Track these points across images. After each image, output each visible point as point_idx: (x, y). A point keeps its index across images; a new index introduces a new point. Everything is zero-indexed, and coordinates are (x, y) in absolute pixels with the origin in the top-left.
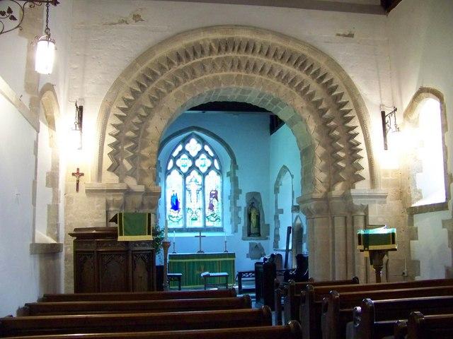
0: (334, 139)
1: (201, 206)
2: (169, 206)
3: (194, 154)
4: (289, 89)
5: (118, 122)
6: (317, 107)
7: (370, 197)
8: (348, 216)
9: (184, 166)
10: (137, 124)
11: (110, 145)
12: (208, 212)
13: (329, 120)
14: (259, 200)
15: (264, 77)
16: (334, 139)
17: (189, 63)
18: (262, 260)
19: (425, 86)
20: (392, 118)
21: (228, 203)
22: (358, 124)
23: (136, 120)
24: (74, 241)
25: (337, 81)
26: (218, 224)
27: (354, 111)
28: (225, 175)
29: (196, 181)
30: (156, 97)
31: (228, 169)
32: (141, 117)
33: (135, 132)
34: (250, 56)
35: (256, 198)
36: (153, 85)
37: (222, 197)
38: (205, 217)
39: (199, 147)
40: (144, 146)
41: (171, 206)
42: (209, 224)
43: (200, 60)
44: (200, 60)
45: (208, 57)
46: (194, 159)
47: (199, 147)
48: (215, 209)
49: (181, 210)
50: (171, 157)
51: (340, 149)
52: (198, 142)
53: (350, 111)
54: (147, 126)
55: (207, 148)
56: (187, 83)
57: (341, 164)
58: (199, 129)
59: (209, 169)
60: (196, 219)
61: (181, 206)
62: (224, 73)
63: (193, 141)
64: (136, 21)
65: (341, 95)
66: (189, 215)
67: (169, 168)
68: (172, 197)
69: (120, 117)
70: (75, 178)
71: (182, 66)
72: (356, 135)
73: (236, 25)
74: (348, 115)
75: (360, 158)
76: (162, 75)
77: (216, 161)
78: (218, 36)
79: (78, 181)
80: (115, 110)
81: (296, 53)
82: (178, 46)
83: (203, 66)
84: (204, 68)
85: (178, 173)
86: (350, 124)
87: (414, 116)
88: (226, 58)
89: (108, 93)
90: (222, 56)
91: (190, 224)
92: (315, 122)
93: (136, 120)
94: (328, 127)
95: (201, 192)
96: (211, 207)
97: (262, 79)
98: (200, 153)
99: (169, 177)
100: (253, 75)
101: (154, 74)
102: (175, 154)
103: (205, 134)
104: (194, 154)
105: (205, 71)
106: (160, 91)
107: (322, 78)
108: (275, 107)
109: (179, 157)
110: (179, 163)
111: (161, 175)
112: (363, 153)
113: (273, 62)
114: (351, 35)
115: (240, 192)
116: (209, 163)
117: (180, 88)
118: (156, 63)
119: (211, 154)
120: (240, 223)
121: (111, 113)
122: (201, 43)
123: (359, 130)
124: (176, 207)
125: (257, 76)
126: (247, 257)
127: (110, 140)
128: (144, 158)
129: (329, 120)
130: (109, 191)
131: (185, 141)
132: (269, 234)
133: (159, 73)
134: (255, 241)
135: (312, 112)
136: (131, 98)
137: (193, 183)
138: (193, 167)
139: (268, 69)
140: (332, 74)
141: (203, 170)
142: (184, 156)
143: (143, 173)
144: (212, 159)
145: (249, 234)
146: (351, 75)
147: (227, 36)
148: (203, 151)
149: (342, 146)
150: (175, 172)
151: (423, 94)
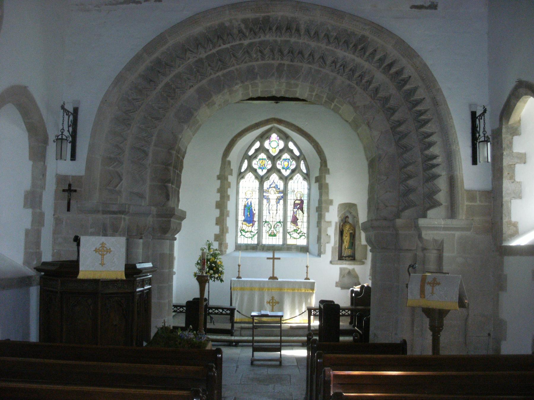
2: (241, 217)
3: (273, 153)
4: (348, 82)
9: (262, 168)
12: (290, 227)
13: (400, 123)
15: (315, 67)
18: (357, 288)
19: (524, 78)
20: (482, 121)
24: (41, 277)
25: (409, 71)
26: (303, 242)
28: (313, 180)
31: (316, 173)
37: (308, 209)
38: (285, 232)
39: (282, 145)
46: (273, 159)
47: (282, 145)
48: (299, 224)
49: (256, 224)
50: (246, 156)
55: (291, 145)
58: (280, 121)
59: (293, 171)
60: (275, 235)
61: (256, 219)
62: (260, 62)
65: (415, 90)
66: (265, 228)
68: (245, 206)
82: (197, 30)
85: (254, 177)
91: (267, 240)
95: (282, 202)
96: (295, 220)
98: (281, 151)
102: (251, 153)
103: (288, 128)
107: (390, 66)
108: (333, 104)
109: (256, 157)
110: (255, 164)
111: (232, 179)
112: (441, 171)
113: (323, 46)
119: (297, 153)
122: (227, 24)
125: (306, 66)
126: (337, 286)
129: (400, 123)
132: (366, 259)
134: (348, 266)
137: (272, 191)
138: (274, 169)
140: (404, 62)
142: (263, 156)
144: (297, 159)
145: (341, 258)
146: (429, 63)
148: (285, 149)
150: (250, 176)
151: (521, 90)
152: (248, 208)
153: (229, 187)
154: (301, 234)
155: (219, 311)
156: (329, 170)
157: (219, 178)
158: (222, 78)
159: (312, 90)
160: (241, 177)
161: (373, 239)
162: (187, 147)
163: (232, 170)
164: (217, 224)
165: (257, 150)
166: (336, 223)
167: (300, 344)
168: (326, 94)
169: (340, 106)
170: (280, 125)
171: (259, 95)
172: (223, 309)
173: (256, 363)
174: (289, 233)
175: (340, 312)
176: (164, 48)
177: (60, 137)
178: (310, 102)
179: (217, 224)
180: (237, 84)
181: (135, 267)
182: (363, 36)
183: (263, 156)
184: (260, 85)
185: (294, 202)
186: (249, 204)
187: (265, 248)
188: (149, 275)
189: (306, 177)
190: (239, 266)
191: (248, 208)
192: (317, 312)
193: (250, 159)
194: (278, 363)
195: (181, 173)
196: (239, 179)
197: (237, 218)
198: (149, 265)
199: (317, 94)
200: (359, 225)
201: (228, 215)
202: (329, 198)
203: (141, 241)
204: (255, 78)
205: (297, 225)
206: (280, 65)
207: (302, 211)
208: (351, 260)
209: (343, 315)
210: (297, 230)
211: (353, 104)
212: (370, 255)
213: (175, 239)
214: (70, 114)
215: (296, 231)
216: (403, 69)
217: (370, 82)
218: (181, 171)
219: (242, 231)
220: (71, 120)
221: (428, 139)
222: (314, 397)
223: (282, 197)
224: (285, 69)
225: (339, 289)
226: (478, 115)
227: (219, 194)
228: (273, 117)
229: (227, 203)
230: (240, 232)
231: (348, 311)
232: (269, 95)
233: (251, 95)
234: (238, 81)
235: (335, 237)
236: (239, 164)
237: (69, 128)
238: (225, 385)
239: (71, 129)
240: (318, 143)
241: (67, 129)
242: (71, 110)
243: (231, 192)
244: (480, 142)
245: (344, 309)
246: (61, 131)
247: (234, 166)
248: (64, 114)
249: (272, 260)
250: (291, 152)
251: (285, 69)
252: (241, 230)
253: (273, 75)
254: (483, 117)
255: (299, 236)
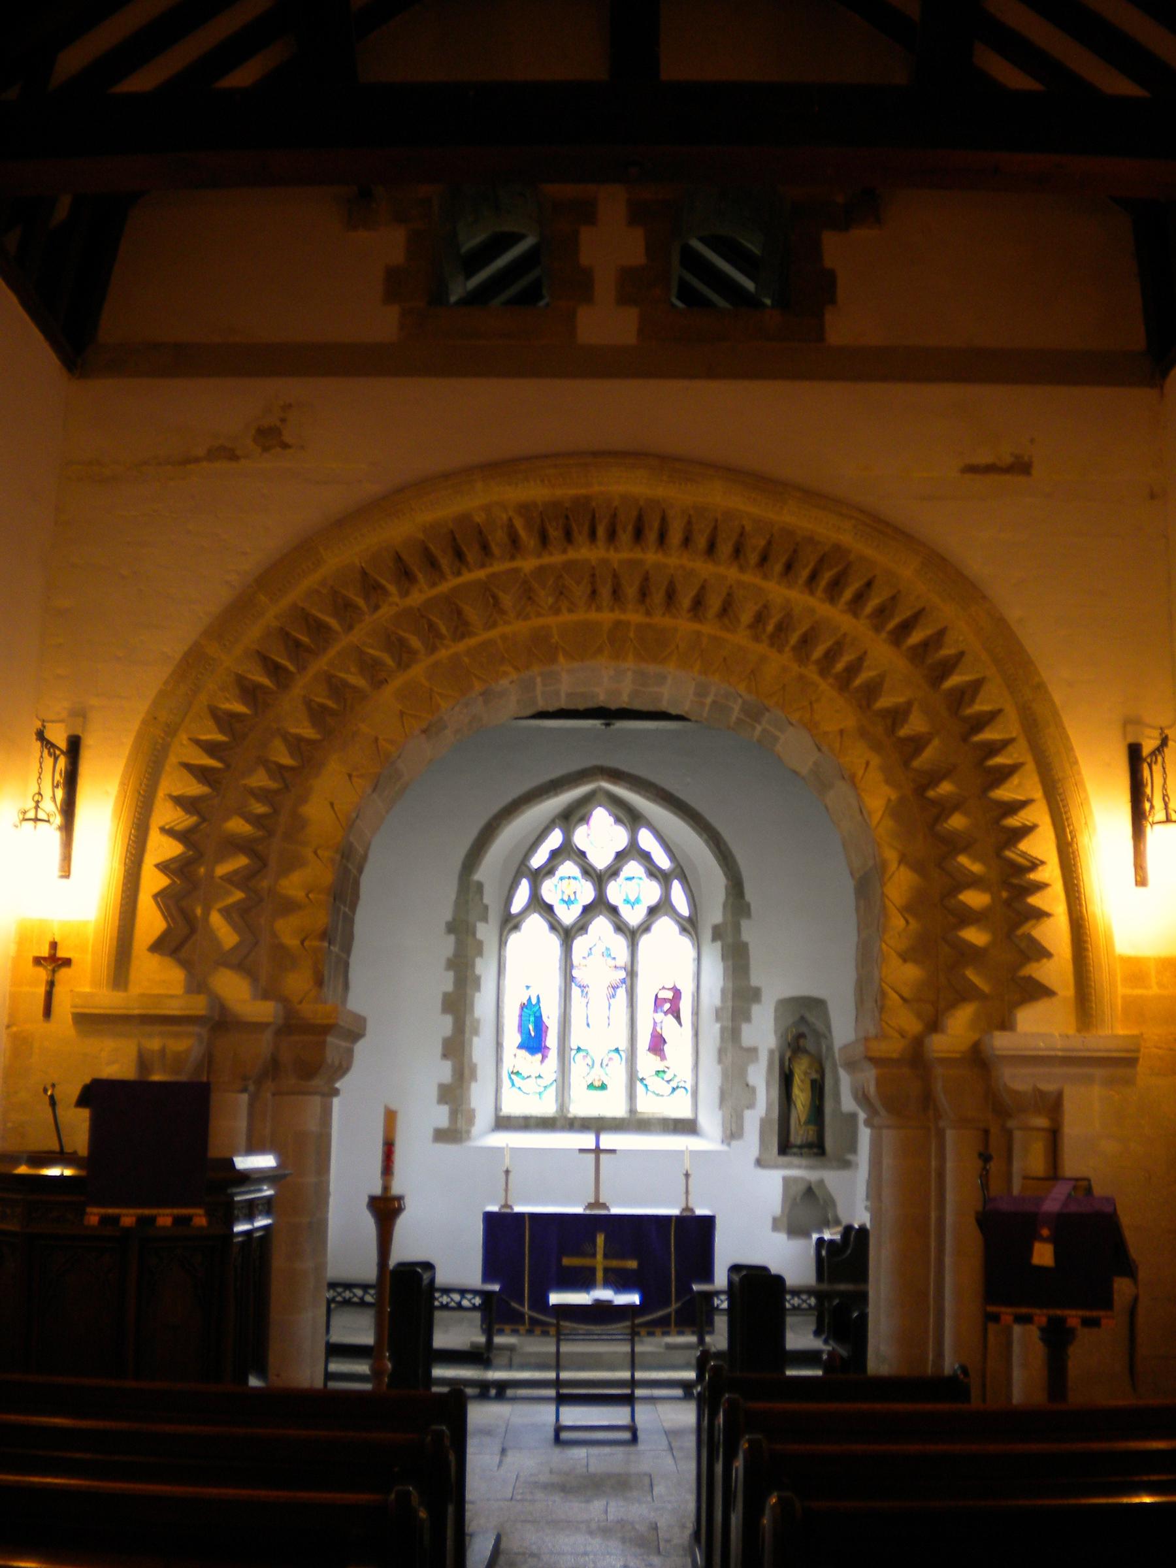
0: (954, 844)
1: (623, 1044)
2: (512, 1037)
3: (601, 860)
4: (795, 668)
5: (195, 789)
6: (892, 729)
7: (1068, 1061)
8: (994, 1130)
10: (263, 795)
11: (163, 867)
12: (647, 1063)
13: (934, 778)
14: (820, 1026)
15: (708, 629)
16: (954, 844)
17: (444, 587)
20: (1157, 768)
21: (712, 1031)
22: (1038, 794)
23: (260, 779)
26: (680, 1108)
27: (1022, 744)
28: (707, 934)
29: (607, 953)
30: (330, 703)
31: (715, 915)
32: (279, 771)
33: (256, 821)
34: (651, 557)
35: (811, 1018)
36: (321, 664)
37: (696, 1013)
38: (633, 1078)
39: (619, 837)
40: (292, 863)
41: (518, 1039)
42: (647, 1106)
43: (481, 574)
44: (481, 574)
45: (508, 565)
46: (600, 879)
47: (619, 837)
49: (553, 1054)
50: (522, 869)
51: (975, 882)
52: (618, 820)
53: (1005, 744)
54: (303, 800)
55: (646, 840)
56: (443, 654)
57: (975, 936)
58: (616, 775)
59: (653, 912)
60: (603, 1087)
61: (552, 1040)
62: (566, 617)
63: (601, 816)
64: (266, 449)
65: (976, 686)
67: (516, 908)
68: (523, 1007)
69: (201, 774)
70: (42, 974)
71: (416, 598)
72: (1026, 831)
73: (595, 454)
74: (999, 760)
75: (1040, 915)
76: (351, 628)
77: (676, 887)
78: (536, 492)
79: (51, 984)
80: (184, 751)
81: (811, 540)
83: (488, 594)
84: (496, 601)
86: (1004, 793)
87: (562, 902)
88: (569, 566)
89: (162, 694)
90: (555, 558)
91: (583, 1105)
92: (887, 782)
93: (260, 779)
94: (933, 802)
95: (622, 993)
96: (657, 1044)
97: (699, 634)
98: (621, 857)
99: (514, 939)
100: (666, 621)
101: (319, 630)
102: (538, 859)
103: (638, 793)
104: (601, 860)
105: (502, 612)
106: (345, 684)
107: (906, 627)
108: (759, 728)
110: (550, 891)
111: (486, 932)
113: (732, 573)
114: (1021, 467)
115: (755, 995)
116: (651, 892)
117: (417, 671)
118: (324, 591)
119: (663, 861)
120: (751, 1106)
121: (173, 760)
122: (479, 518)
123: (1038, 814)
124: (534, 1043)
125: (683, 625)
127: (162, 848)
128: (288, 907)
130: (147, 1020)
131: (571, 817)
133: (333, 623)
135: (877, 747)
136: (239, 708)
138: (600, 905)
139: (714, 603)
140: (947, 612)
141: (633, 917)
142: (568, 868)
143: (282, 958)
144: (663, 878)
145: (785, 1148)
147: (566, 492)
148: (632, 851)
149: (976, 868)
150: (535, 923)
152: (531, 1012)
153: (480, 953)
154: (673, 1084)
155: (452, 1300)
156: (748, 905)
157: (451, 928)
158: (466, 660)
159: (701, 692)
160: (510, 925)
161: (872, 1090)
162: (369, 844)
163: (486, 907)
164: (445, 1056)
165: (555, 854)
166: (771, 1052)
167: (678, 1392)
168: (740, 701)
169: (778, 733)
170: (615, 783)
171: (563, 703)
172: (463, 1292)
173: (565, 1435)
174: (642, 1080)
175: (785, 1299)
176: (311, 581)
177: (31, 815)
178: (696, 721)
179: (445, 1056)
180: (505, 674)
181: (232, 1163)
182: (837, 548)
183: (568, 868)
184: (564, 676)
185: (656, 996)
186: (534, 1001)
187: (576, 1124)
188: (266, 1190)
189: (688, 926)
190: (507, 1172)
191: (531, 1012)
192: (722, 1301)
193: (537, 877)
194: (626, 1435)
195: (354, 912)
196: (505, 933)
197: (500, 1041)
198: (266, 1161)
199: (714, 702)
200: (833, 1057)
201: (476, 1032)
202: (749, 981)
203: (244, 1097)
204: (553, 660)
205: (663, 1057)
206: (618, 624)
207: (678, 1018)
208: (816, 1155)
209: (795, 1309)
210: (664, 1072)
211: (811, 727)
212: (865, 1135)
213: (336, 1092)
214: (58, 752)
215: (661, 1074)
216: (941, 634)
217: (853, 669)
218: (353, 906)
219: (513, 1076)
220: (61, 771)
221: (1016, 817)
222: (717, 1559)
223: (623, 981)
224: (632, 635)
225: (781, 1237)
226: (1146, 751)
227: (451, 974)
228: (598, 763)
229: (473, 997)
230: (510, 1078)
231: (809, 1298)
232: (591, 704)
233: (541, 705)
234: (509, 669)
235: (768, 1090)
236: (506, 892)
237: (56, 790)
238: (472, 1503)
239: (60, 794)
240: (718, 833)
241: (51, 795)
242: (63, 745)
243: (485, 969)
244: (1153, 824)
245: (796, 1293)
246: (33, 799)
247: (490, 897)
248: (42, 753)
249: (592, 1156)
250: (646, 857)
251: (632, 635)
252: (512, 1072)
253: (600, 650)
254: (1160, 759)
255: (669, 1088)
